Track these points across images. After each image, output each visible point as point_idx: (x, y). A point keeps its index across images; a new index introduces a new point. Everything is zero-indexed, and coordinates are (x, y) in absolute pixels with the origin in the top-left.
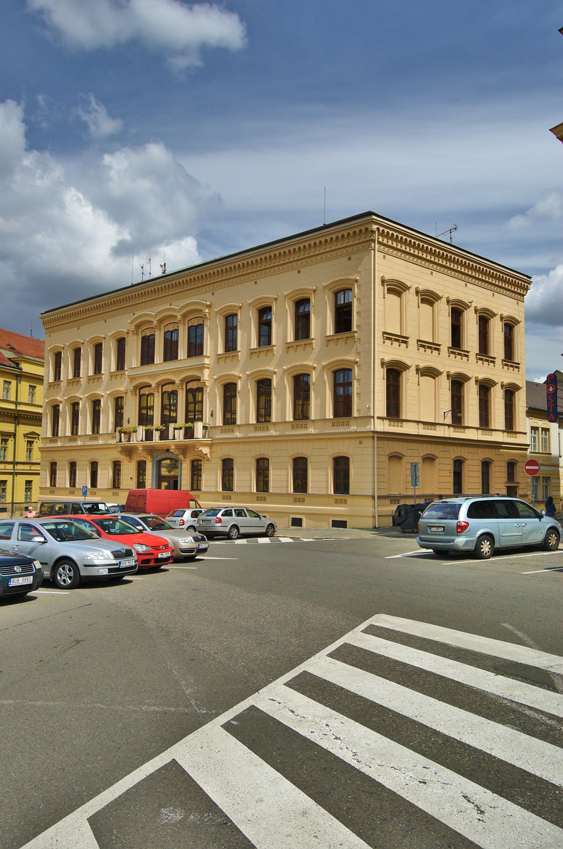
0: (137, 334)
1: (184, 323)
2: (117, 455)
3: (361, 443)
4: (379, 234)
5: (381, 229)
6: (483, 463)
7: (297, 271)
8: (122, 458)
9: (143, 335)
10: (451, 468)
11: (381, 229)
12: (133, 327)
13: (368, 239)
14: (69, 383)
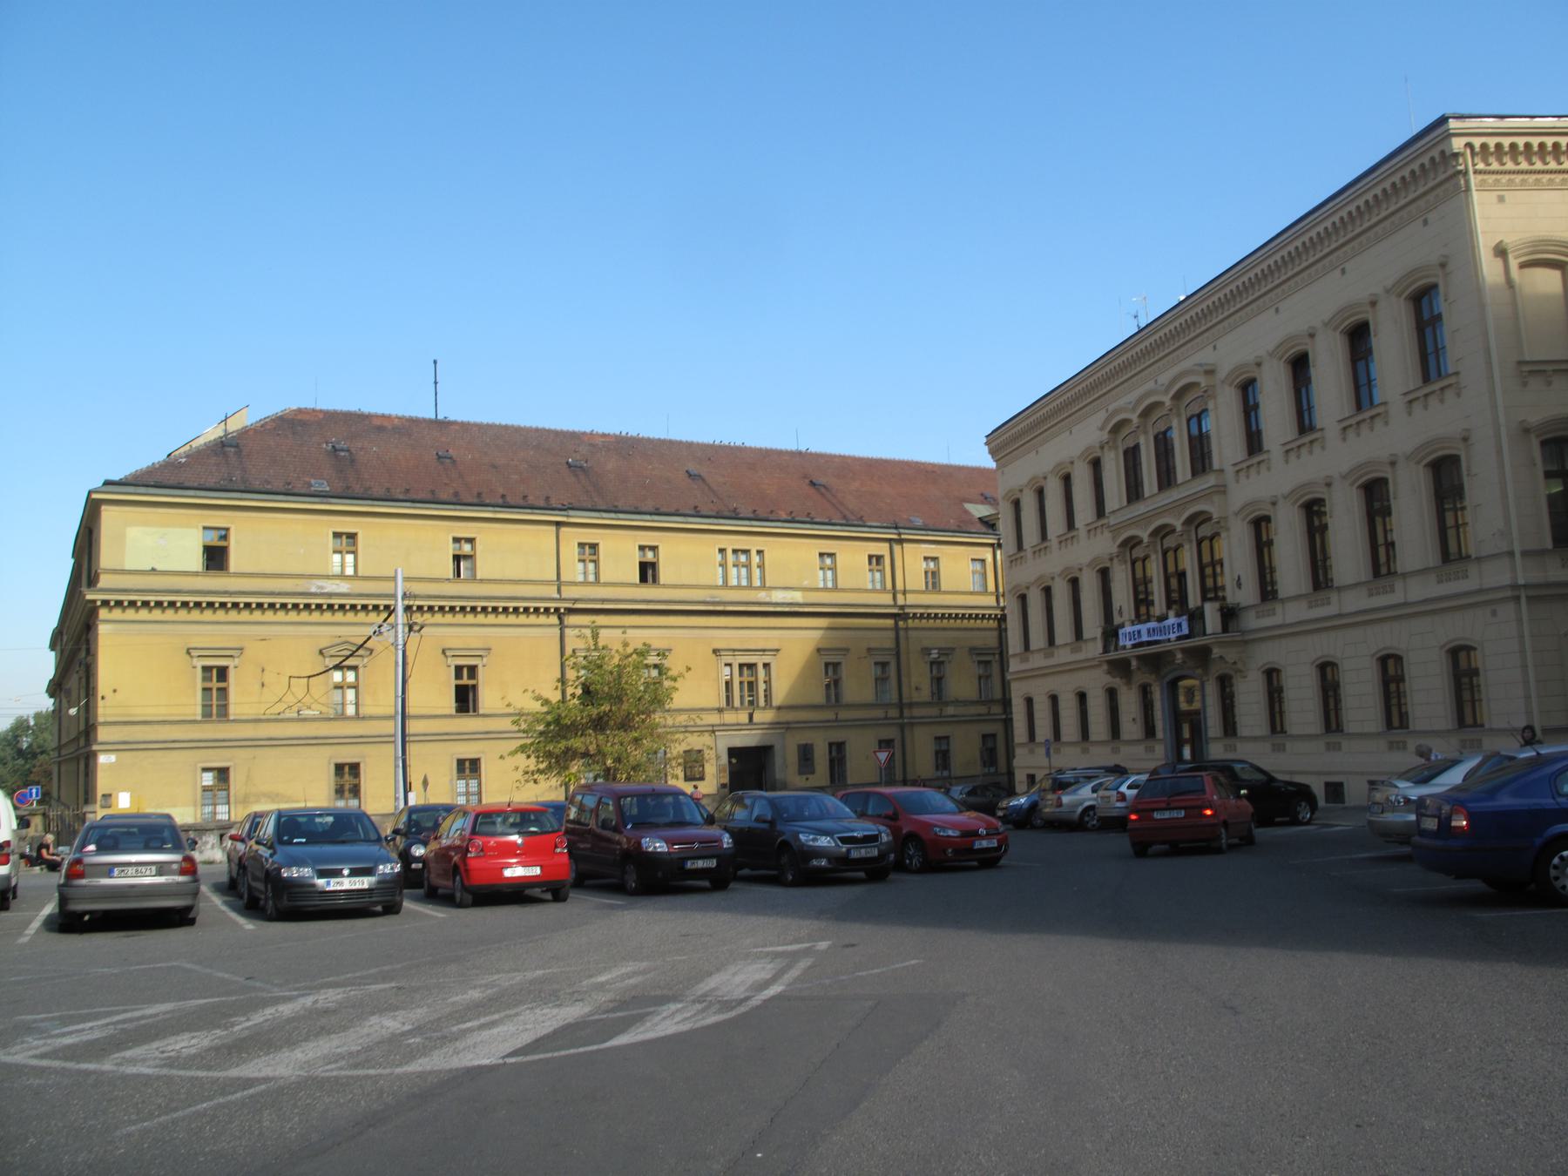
0: (1116, 448)
1: (1146, 433)
3: (1494, 613)
4: (1473, 154)
7: (1420, 221)
8: (1117, 682)
11: (1477, 142)
12: (1105, 436)
13: (1450, 172)
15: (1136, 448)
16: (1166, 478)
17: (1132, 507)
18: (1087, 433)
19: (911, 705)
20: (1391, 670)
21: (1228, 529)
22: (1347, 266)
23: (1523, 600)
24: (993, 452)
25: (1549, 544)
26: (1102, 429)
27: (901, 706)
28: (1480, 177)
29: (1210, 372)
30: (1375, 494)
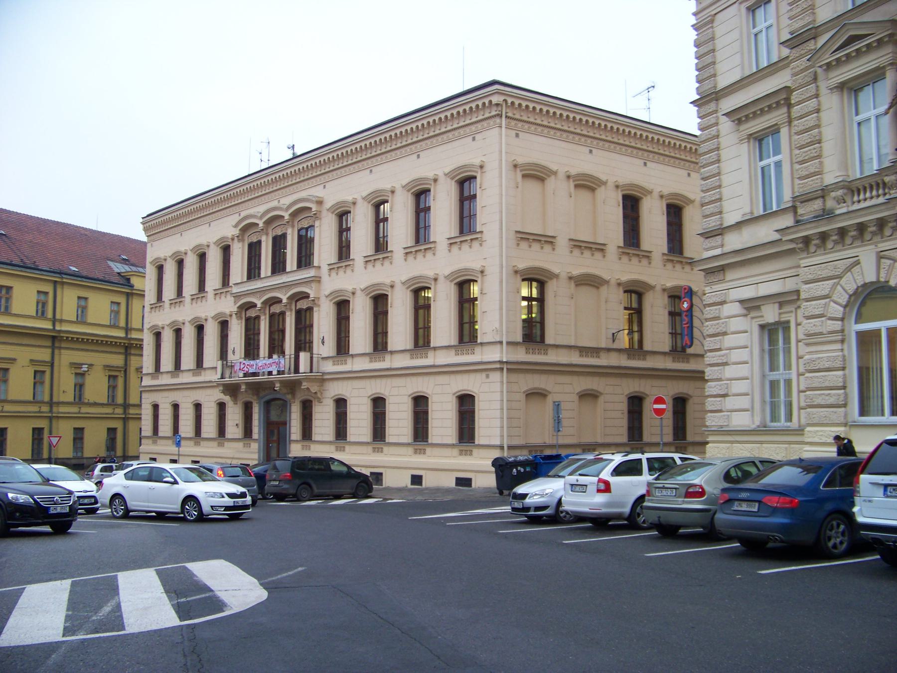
1: (293, 226)
2: (217, 395)
3: (487, 376)
5: (510, 100)
6: (629, 398)
8: (227, 399)
9: (274, 234)
10: (624, 406)
12: (236, 232)
14: (192, 299)
15: (284, 236)
16: (278, 266)
17: (248, 284)
18: (226, 227)
19: (59, 403)
20: (420, 403)
21: (319, 306)
22: (421, 154)
23: (505, 370)
24: (146, 230)
25: (519, 338)
26: (236, 226)
27: (51, 404)
28: (508, 120)
29: (320, 203)
30: (380, 303)
